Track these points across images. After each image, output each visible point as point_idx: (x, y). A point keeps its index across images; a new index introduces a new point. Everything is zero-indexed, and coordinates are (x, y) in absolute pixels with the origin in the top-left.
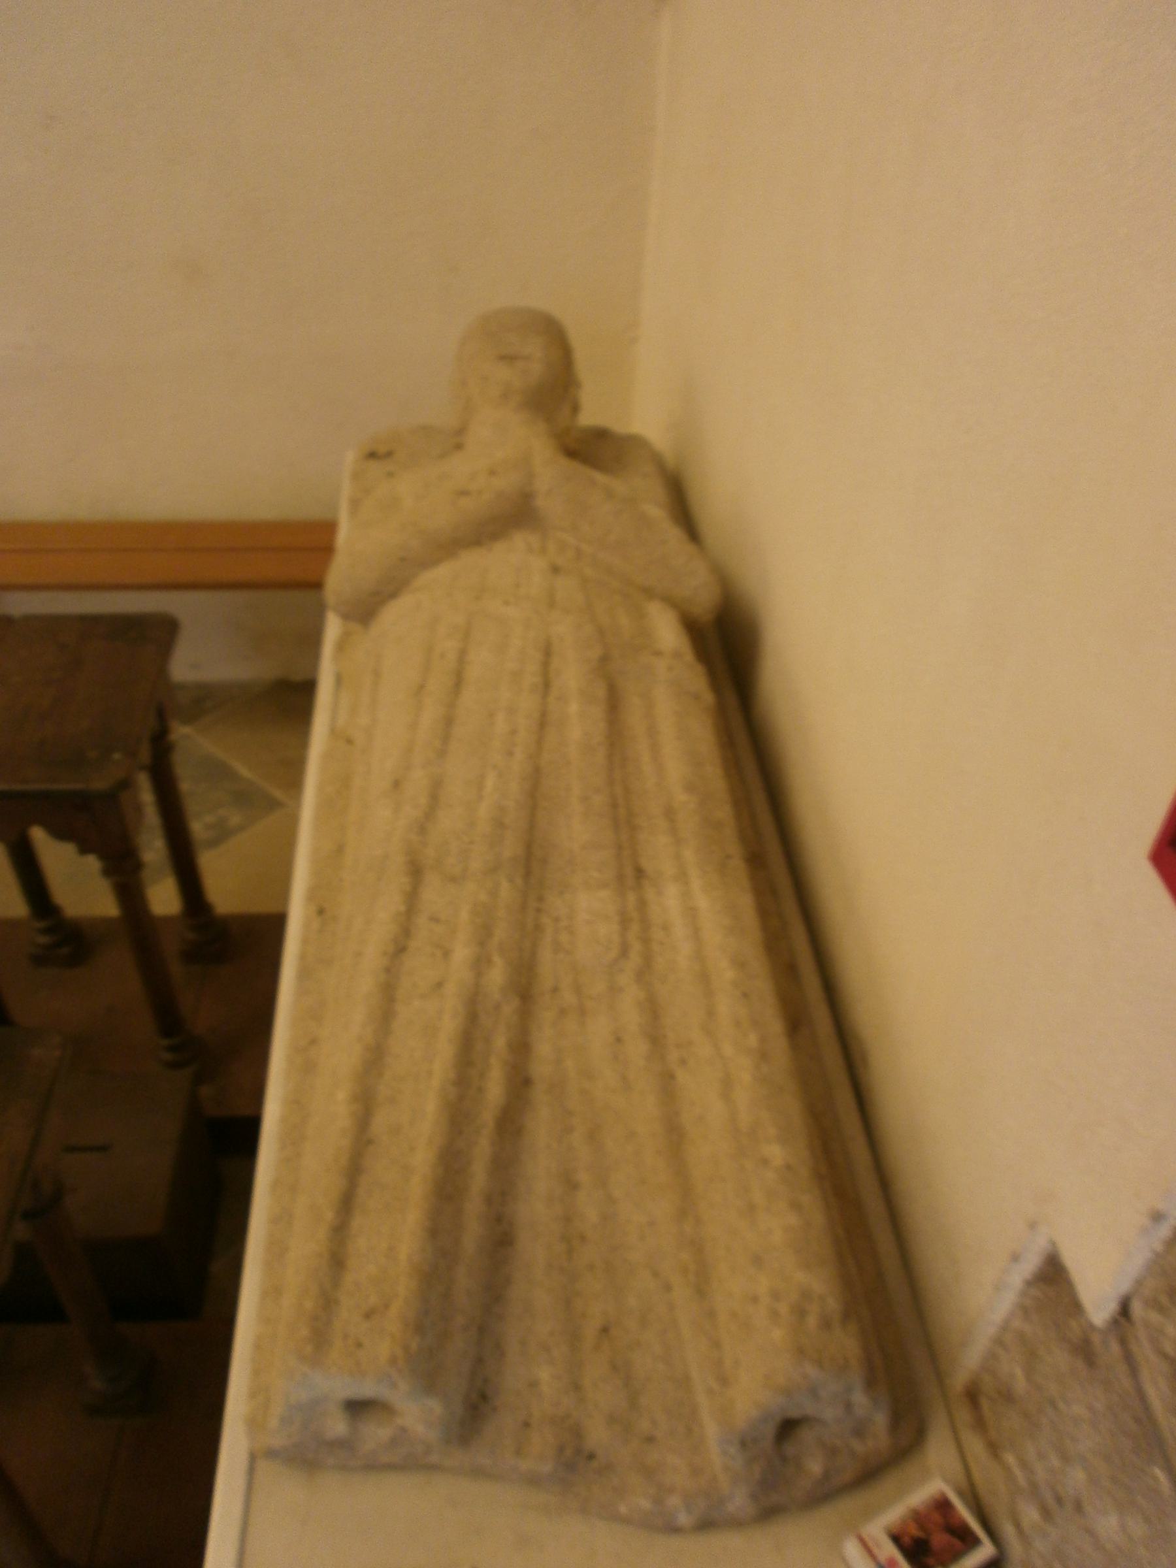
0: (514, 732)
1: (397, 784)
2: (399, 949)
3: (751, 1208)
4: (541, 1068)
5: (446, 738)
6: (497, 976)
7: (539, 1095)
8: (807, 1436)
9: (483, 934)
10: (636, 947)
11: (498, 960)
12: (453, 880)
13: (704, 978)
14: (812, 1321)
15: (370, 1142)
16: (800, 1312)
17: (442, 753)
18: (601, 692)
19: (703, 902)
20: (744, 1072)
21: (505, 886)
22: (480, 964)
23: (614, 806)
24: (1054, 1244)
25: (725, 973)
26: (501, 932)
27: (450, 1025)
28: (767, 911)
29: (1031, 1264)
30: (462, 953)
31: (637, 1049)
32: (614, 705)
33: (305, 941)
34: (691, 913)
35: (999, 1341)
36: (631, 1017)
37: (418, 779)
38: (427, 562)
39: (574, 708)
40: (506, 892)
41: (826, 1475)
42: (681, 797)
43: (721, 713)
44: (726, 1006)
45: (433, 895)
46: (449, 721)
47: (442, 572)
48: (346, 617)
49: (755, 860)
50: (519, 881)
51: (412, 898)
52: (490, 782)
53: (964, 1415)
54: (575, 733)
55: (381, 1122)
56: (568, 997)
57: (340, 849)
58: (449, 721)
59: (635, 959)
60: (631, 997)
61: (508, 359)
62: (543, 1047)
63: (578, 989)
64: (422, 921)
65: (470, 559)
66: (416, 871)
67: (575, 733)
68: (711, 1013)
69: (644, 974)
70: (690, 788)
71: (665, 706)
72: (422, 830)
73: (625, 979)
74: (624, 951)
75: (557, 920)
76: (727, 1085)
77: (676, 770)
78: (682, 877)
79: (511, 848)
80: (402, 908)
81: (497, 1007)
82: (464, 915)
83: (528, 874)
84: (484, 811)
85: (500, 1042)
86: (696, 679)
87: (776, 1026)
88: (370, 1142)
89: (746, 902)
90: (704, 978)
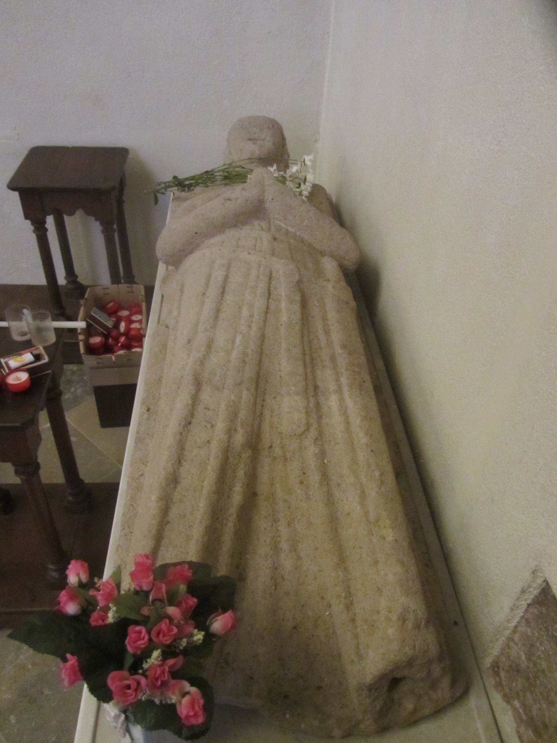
0: (251, 316)
1: (189, 341)
2: (188, 423)
3: (376, 562)
4: (263, 488)
5: (216, 318)
6: (239, 438)
7: (263, 508)
8: (404, 687)
9: (233, 416)
10: (315, 426)
11: (241, 431)
12: (217, 389)
13: (351, 442)
14: (410, 625)
15: (168, 522)
16: (403, 620)
17: (214, 326)
18: (298, 298)
19: (349, 403)
20: (372, 491)
21: (245, 392)
22: (230, 432)
23: (304, 354)
24: (546, 581)
25: (362, 439)
26: (243, 414)
27: (213, 464)
28: (384, 414)
29: (534, 592)
30: (221, 426)
31: (314, 478)
32: (304, 304)
33: (140, 424)
34: (344, 413)
35: (510, 639)
36: (312, 462)
37: (201, 338)
38: (207, 235)
39: (283, 304)
40: (246, 395)
41: (415, 711)
42: (339, 350)
43: (360, 318)
44: (362, 456)
45: (206, 396)
46: (218, 311)
47: (217, 239)
48: (167, 263)
49: (378, 390)
50: (253, 390)
51: (195, 398)
52: (238, 341)
53: (490, 682)
54: (284, 318)
55: (174, 512)
56: (278, 451)
57: (160, 380)
58: (218, 311)
59: (313, 433)
60: (311, 450)
61: (252, 140)
62: (264, 476)
63: (283, 447)
64: (201, 407)
65: (231, 233)
66: (198, 384)
67: (284, 318)
68: (354, 461)
69: (320, 438)
70: (344, 347)
71: (332, 315)
72: (202, 364)
73: (308, 442)
74: (308, 426)
75: (272, 411)
76: (363, 495)
77: (337, 336)
78: (339, 391)
79: (249, 372)
80: (190, 402)
81: (239, 456)
82: (223, 407)
83: (257, 387)
84: (234, 355)
85: (241, 473)
86: (347, 294)
87: (390, 477)
88: (168, 522)
89: (374, 405)
90: (351, 442)
